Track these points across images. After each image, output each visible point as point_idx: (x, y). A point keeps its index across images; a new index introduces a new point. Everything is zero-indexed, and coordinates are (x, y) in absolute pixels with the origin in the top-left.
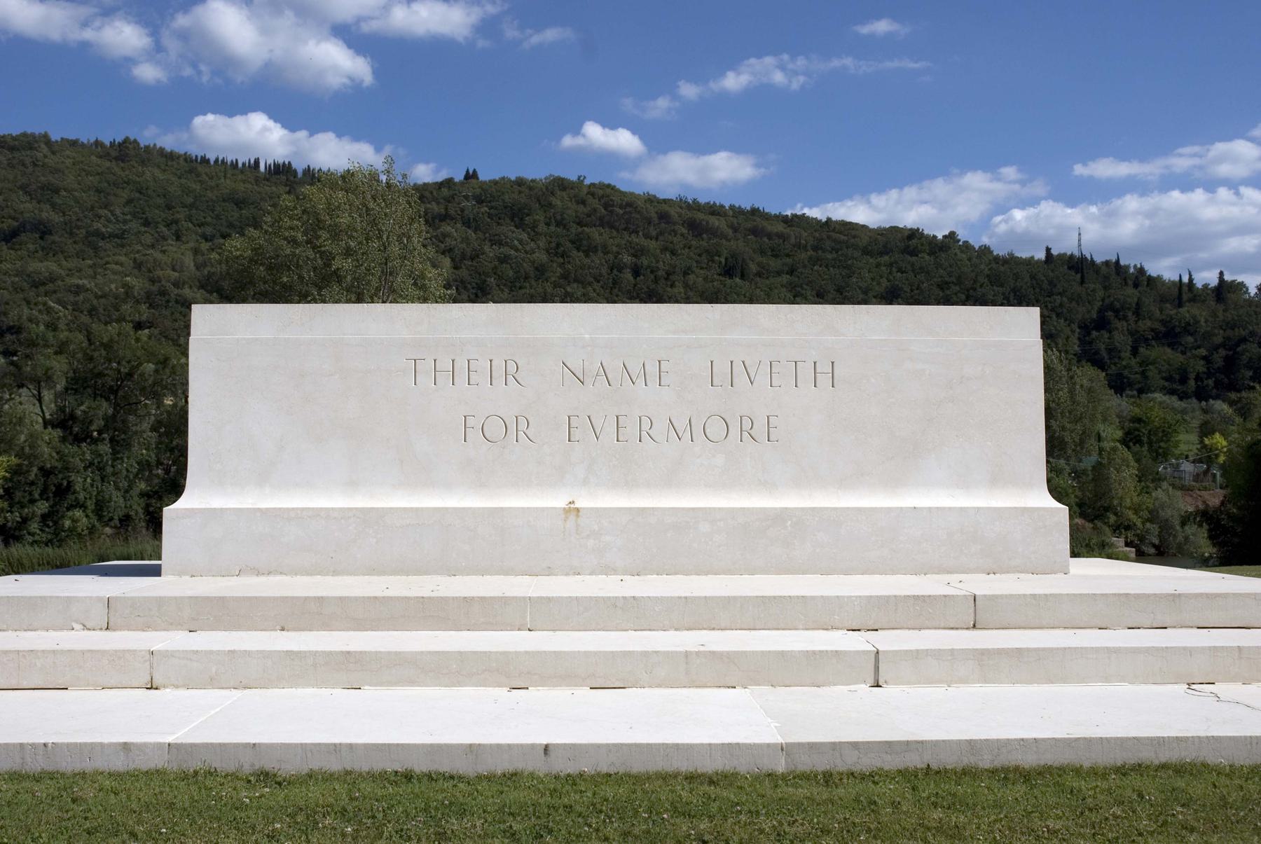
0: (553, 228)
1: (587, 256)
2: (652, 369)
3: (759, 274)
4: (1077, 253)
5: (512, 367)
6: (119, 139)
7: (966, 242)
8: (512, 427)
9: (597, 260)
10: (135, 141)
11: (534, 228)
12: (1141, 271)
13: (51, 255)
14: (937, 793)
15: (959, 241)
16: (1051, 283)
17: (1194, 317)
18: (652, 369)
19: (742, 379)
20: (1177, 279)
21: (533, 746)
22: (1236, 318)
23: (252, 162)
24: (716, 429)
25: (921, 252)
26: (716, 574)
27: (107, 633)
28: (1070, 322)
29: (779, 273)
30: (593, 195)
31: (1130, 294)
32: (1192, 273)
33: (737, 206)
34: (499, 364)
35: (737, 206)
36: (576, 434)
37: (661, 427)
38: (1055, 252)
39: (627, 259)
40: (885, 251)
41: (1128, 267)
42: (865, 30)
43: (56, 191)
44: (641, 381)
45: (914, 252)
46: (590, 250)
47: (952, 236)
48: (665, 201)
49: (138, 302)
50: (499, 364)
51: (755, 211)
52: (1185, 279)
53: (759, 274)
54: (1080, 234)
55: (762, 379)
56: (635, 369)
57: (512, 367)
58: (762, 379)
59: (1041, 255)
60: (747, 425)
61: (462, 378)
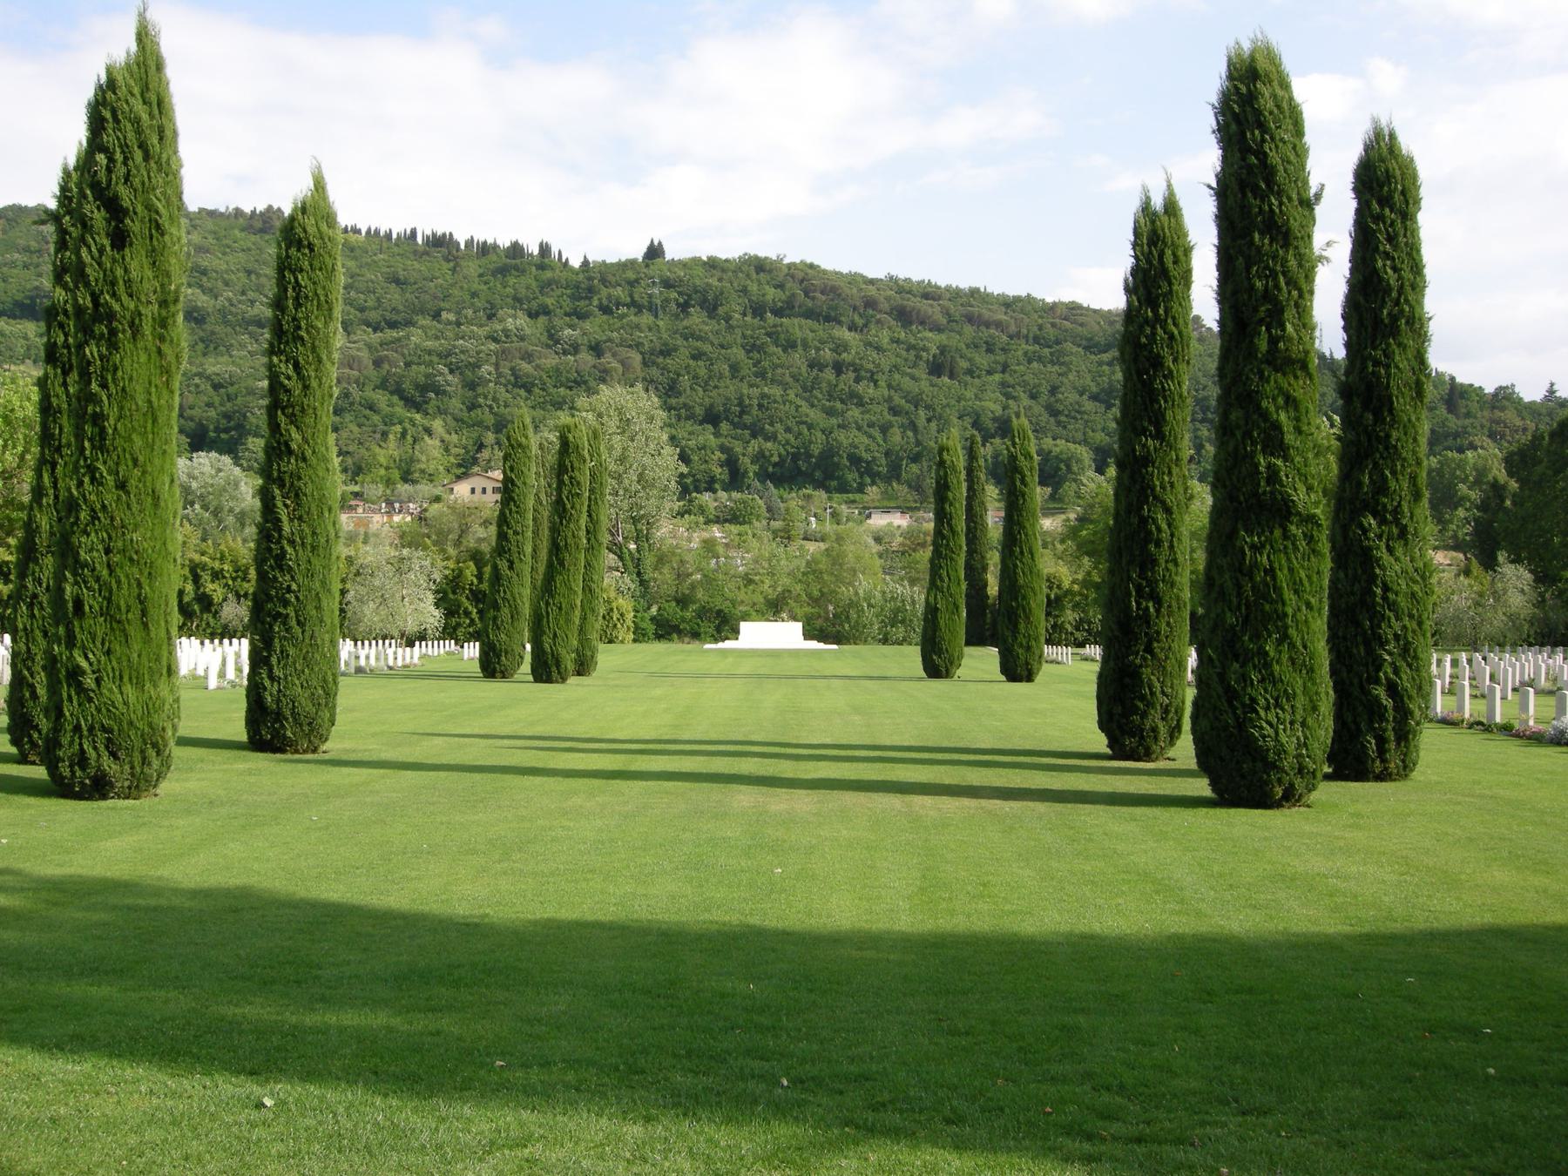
0: (748, 319)
1: (785, 351)
3: (970, 372)
6: (261, 207)
9: (798, 359)
11: (728, 319)
14: (958, 402)
23: (408, 232)
30: (793, 277)
46: (790, 345)
48: (872, 282)
51: (974, 292)
53: (970, 372)
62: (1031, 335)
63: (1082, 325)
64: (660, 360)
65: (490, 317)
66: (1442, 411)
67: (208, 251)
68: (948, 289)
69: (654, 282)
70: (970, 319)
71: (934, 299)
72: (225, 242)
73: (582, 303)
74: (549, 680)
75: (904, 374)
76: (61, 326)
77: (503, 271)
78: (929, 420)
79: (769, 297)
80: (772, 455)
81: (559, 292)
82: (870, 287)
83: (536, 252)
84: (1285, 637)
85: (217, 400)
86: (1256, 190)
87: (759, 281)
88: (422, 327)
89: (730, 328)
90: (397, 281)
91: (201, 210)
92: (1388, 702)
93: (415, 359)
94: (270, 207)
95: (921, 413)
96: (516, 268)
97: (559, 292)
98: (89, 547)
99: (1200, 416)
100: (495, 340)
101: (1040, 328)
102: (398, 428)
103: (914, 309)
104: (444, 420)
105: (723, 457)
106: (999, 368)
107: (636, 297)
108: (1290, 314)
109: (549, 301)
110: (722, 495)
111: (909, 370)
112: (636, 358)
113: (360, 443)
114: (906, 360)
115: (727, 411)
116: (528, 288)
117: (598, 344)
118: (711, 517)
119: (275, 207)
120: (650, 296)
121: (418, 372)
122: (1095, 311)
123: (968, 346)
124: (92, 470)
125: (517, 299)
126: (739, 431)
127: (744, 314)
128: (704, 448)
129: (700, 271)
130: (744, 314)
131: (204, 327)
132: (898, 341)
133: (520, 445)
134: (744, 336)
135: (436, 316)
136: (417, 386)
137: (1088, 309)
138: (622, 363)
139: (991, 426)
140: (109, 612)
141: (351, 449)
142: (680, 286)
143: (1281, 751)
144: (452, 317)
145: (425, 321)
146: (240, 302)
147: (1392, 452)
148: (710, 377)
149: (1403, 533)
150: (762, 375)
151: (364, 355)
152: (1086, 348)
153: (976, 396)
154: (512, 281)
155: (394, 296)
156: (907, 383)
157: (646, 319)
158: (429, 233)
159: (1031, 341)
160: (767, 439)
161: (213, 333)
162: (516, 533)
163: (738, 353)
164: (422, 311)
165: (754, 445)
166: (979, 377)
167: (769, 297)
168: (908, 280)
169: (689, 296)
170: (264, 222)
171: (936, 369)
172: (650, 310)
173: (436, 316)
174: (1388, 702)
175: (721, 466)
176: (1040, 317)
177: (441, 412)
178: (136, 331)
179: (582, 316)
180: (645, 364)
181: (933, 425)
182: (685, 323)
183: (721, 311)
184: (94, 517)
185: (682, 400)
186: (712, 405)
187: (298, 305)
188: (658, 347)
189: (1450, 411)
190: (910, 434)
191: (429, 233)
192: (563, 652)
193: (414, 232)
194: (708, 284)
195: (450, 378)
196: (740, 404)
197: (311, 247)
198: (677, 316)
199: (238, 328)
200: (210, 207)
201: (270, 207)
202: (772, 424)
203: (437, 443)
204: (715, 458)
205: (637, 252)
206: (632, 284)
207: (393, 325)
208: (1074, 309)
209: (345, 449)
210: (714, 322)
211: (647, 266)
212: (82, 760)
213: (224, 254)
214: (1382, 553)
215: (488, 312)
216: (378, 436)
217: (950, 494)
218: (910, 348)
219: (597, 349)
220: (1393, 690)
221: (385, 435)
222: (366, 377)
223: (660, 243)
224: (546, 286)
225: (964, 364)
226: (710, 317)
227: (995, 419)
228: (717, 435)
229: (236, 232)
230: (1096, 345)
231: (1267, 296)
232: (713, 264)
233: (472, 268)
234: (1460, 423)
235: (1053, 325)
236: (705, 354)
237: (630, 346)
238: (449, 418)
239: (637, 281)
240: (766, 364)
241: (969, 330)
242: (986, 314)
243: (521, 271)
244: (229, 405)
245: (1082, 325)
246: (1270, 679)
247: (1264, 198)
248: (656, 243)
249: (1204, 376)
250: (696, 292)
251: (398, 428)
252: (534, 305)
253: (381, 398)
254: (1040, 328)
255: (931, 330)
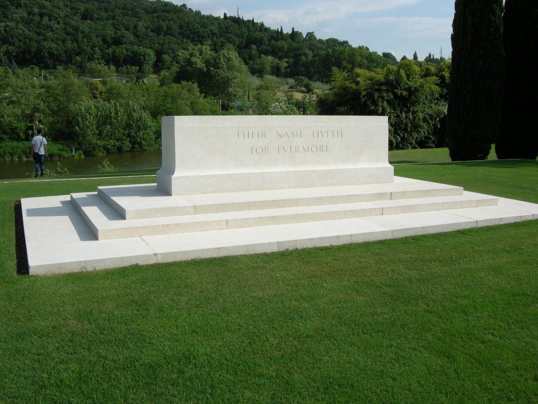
2: (299, 133)
4: (237, 16)
5: (264, 133)
7: (190, 9)
8: (264, 150)
12: (262, 25)
15: (187, 8)
17: (283, 46)
18: (299, 133)
19: (320, 136)
20: (277, 29)
21: (349, 235)
22: (299, 47)
24: (314, 149)
25: (171, 12)
27: (383, 216)
29: (107, 19)
31: (258, 35)
32: (283, 28)
34: (260, 133)
36: (280, 151)
37: (301, 148)
38: (228, 16)
39: (36, 10)
40: (155, 11)
41: (257, 23)
42: (493, 146)
44: (296, 137)
45: (168, 12)
47: (184, 5)
50: (260, 133)
52: (280, 30)
54: (238, 9)
55: (325, 136)
56: (295, 133)
57: (264, 133)
58: (325, 136)
59: (222, 17)
60: (321, 148)
61: (251, 136)
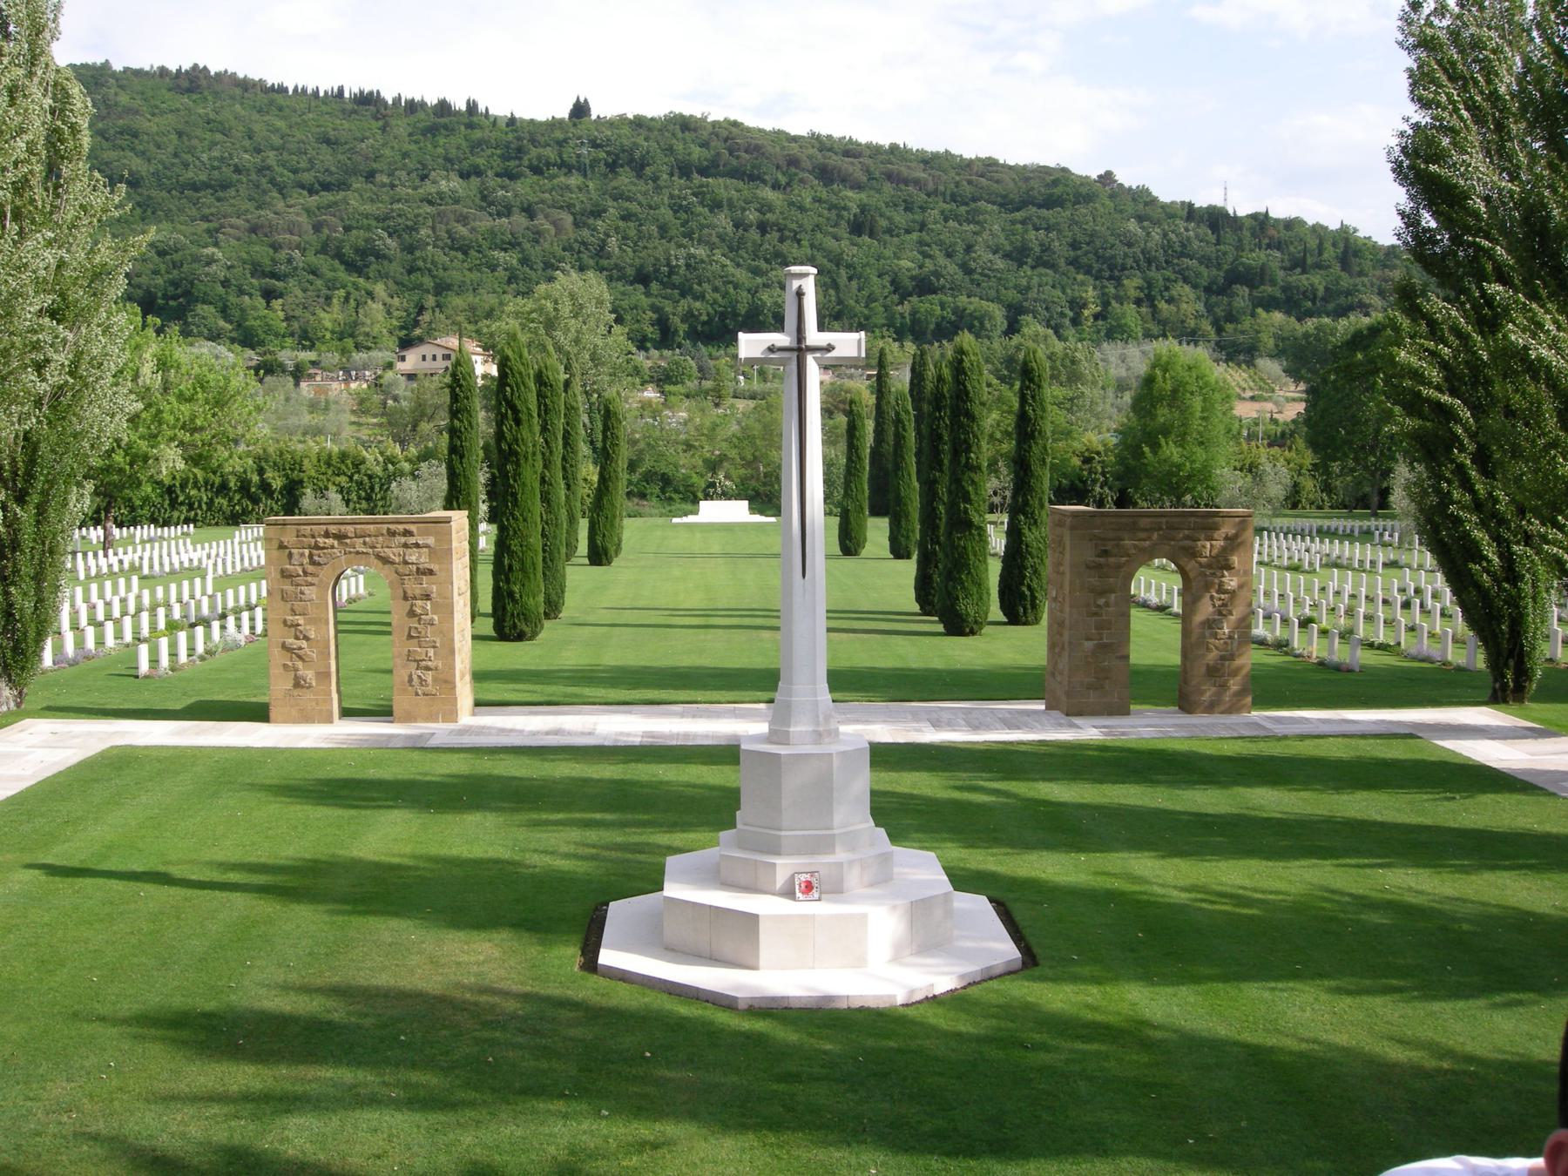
3: (889, 231)
6: (186, 66)
10: (205, 68)
11: (655, 179)
13: (149, 212)
16: (1183, 245)
23: (336, 90)
26: (1004, 1148)
28: (1195, 287)
33: (460, 105)
35: (460, 105)
43: (135, 135)
47: (1107, 178)
48: (795, 139)
49: (284, 336)
51: (894, 148)
62: (948, 192)
63: (997, 182)
64: (591, 221)
65: (423, 178)
66: (1336, 269)
67: (137, 112)
68: (869, 146)
69: (582, 143)
70: (889, 176)
71: (855, 156)
72: (153, 102)
73: (512, 163)
74: (600, 564)
75: (826, 234)
76: (459, 437)
77: (432, 130)
78: (850, 279)
79: (695, 156)
80: (701, 314)
81: (489, 152)
82: (793, 145)
83: (464, 108)
84: (969, 573)
85: (163, 267)
86: (962, 400)
87: (684, 139)
88: (356, 190)
89: (658, 189)
90: (328, 141)
91: (126, 70)
92: (1027, 593)
93: (354, 223)
94: (196, 66)
95: (843, 272)
96: (446, 127)
97: (489, 152)
98: (514, 545)
99: (1107, 274)
100: (430, 203)
101: (957, 184)
102: (342, 293)
103: (835, 168)
104: (386, 284)
105: (655, 316)
106: (917, 227)
107: (565, 156)
108: (974, 448)
109: (481, 161)
110: (655, 353)
111: (831, 230)
112: (568, 219)
113: (305, 308)
114: (828, 219)
115: (657, 271)
116: (458, 148)
117: (530, 205)
118: (646, 378)
119: (201, 66)
120: (579, 156)
121: (358, 237)
122: (1011, 168)
123: (887, 205)
124: (512, 515)
125: (447, 159)
126: (669, 291)
127: (672, 175)
128: (636, 307)
129: (626, 131)
130: (672, 175)
131: (140, 190)
132: (819, 201)
133: (573, 408)
134: (671, 197)
135: (370, 176)
136: (357, 251)
137: (1005, 166)
138: (554, 223)
139: (909, 284)
140: (523, 569)
141: (297, 313)
142: (607, 145)
143: (968, 614)
144: (385, 180)
145: (358, 183)
146: (173, 164)
147: (1031, 490)
148: (640, 238)
149: (1036, 522)
150: (689, 235)
151: (303, 219)
152: (1001, 205)
153: (895, 253)
154: (442, 141)
155: (326, 157)
156: (830, 243)
157: (574, 180)
158: (357, 91)
159: (948, 198)
160: (696, 298)
161: (149, 197)
162: (571, 466)
163: (666, 213)
164: (354, 172)
165: (684, 304)
166: (898, 236)
167: (695, 156)
168: (829, 137)
169: (617, 156)
170: (191, 82)
171: (857, 228)
172: (579, 170)
173: (370, 176)
174: (1027, 593)
175: (653, 325)
176: (958, 174)
177: (383, 276)
178: (527, 459)
179: (513, 177)
180: (576, 224)
181: (854, 283)
182: (614, 184)
183: (648, 171)
184: (515, 532)
185: (612, 262)
186: (642, 266)
187: (546, 414)
188: (589, 207)
189: (1343, 269)
190: (832, 292)
191: (357, 91)
192: (609, 545)
193: (341, 90)
194: (634, 143)
195: (389, 241)
196: (668, 265)
197: (551, 386)
198: (605, 176)
199: (174, 192)
200: (135, 66)
201: (196, 66)
202: (700, 284)
203: (381, 307)
204: (647, 317)
205: (563, 112)
206: (561, 143)
207: (326, 187)
208: (990, 165)
209: (291, 313)
210: (642, 182)
211: (575, 125)
212: (515, 626)
213: (153, 115)
214: (1026, 531)
215: (420, 172)
216: (322, 300)
217: (857, 434)
218: (832, 207)
219: (529, 211)
220: (1029, 588)
221: (328, 299)
222: (307, 243)
223: (586, 100)
224: (476, 146)
225: (883, 223)
226: (639, 176)
227: (913, 278)
228: (648, 294)
229: (164, 91)
230: (1011, 202)
231: (966, 441)
232: (639, 123)
233: (401, 127)
234: (1351, 281)
235: (970, 182)
236: (635, 215)
237: (561, 208)
238: (391, 283)
239: (565, 141)
240: (693, 224)
241: (888, 188)
242: (905, 172)
243: (450, 130)
244: (175, 272)
245: (997, 182)
246: (963, 588)
247: (965, 403)
248: (582, 100)
249: (1112, 235)
250: (624, 151)
251: (342, 293)
252: (465, 164)
253: (323, 263)
254: (957, 184)
255: (852, 188)
